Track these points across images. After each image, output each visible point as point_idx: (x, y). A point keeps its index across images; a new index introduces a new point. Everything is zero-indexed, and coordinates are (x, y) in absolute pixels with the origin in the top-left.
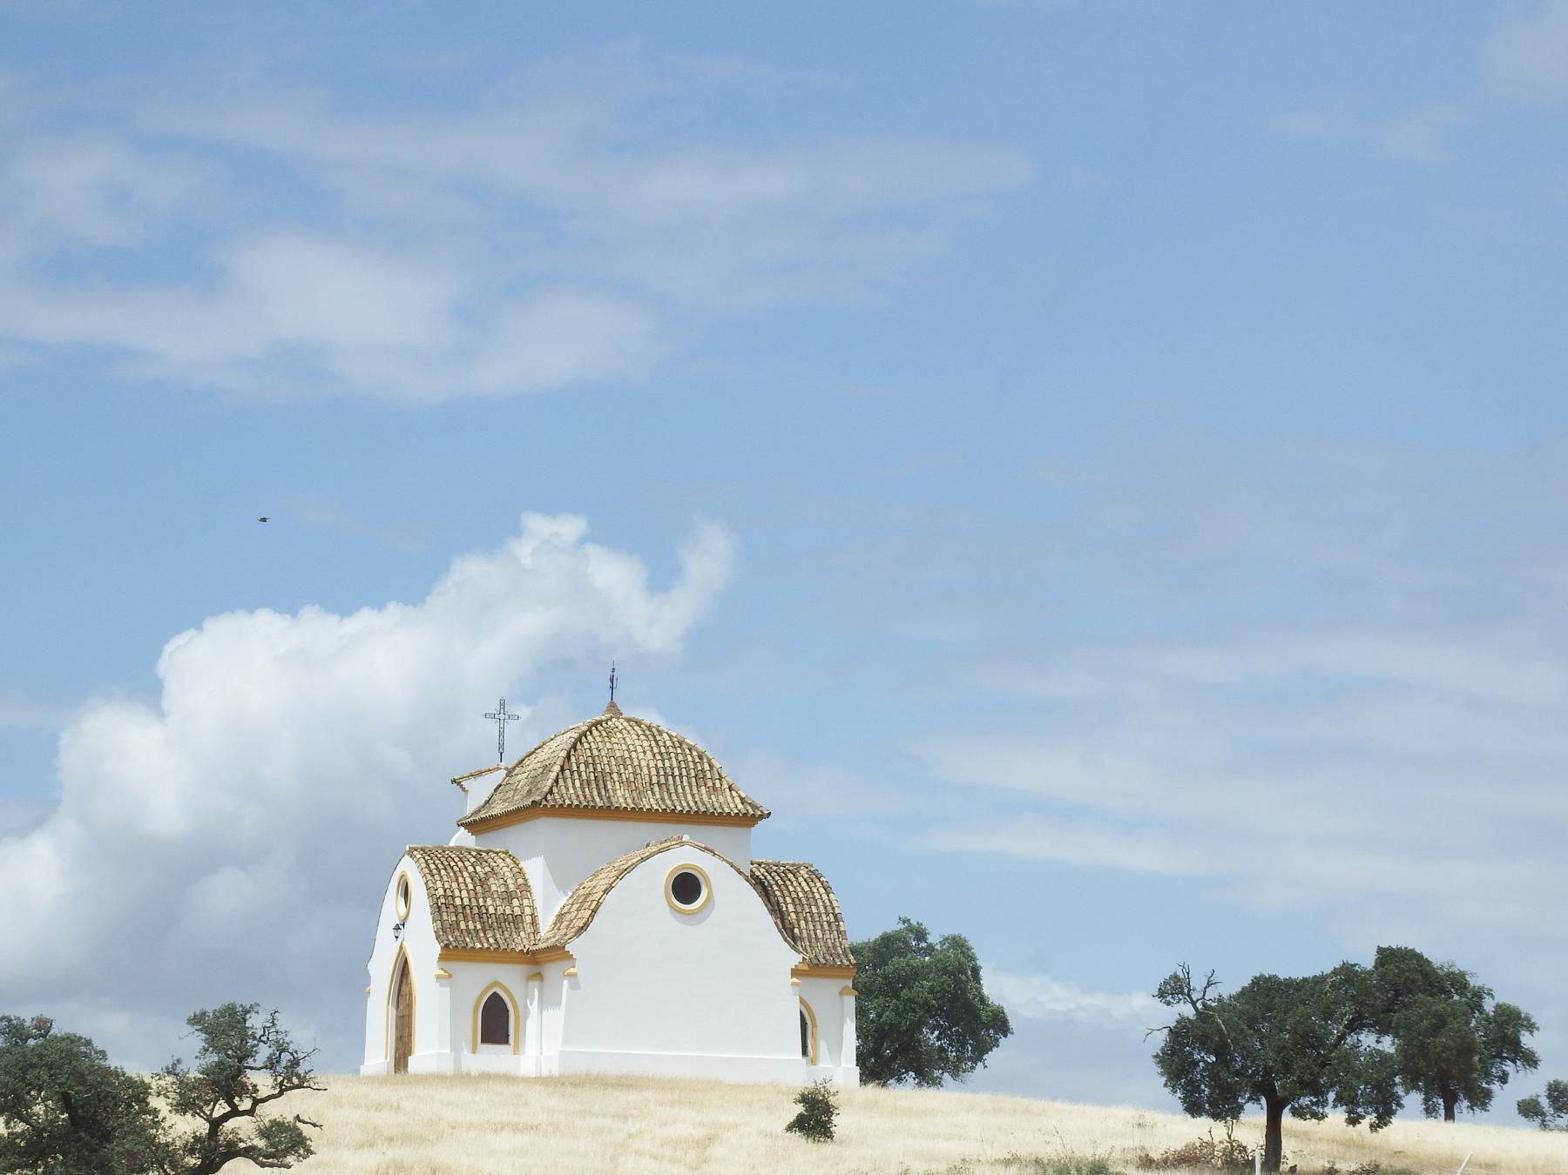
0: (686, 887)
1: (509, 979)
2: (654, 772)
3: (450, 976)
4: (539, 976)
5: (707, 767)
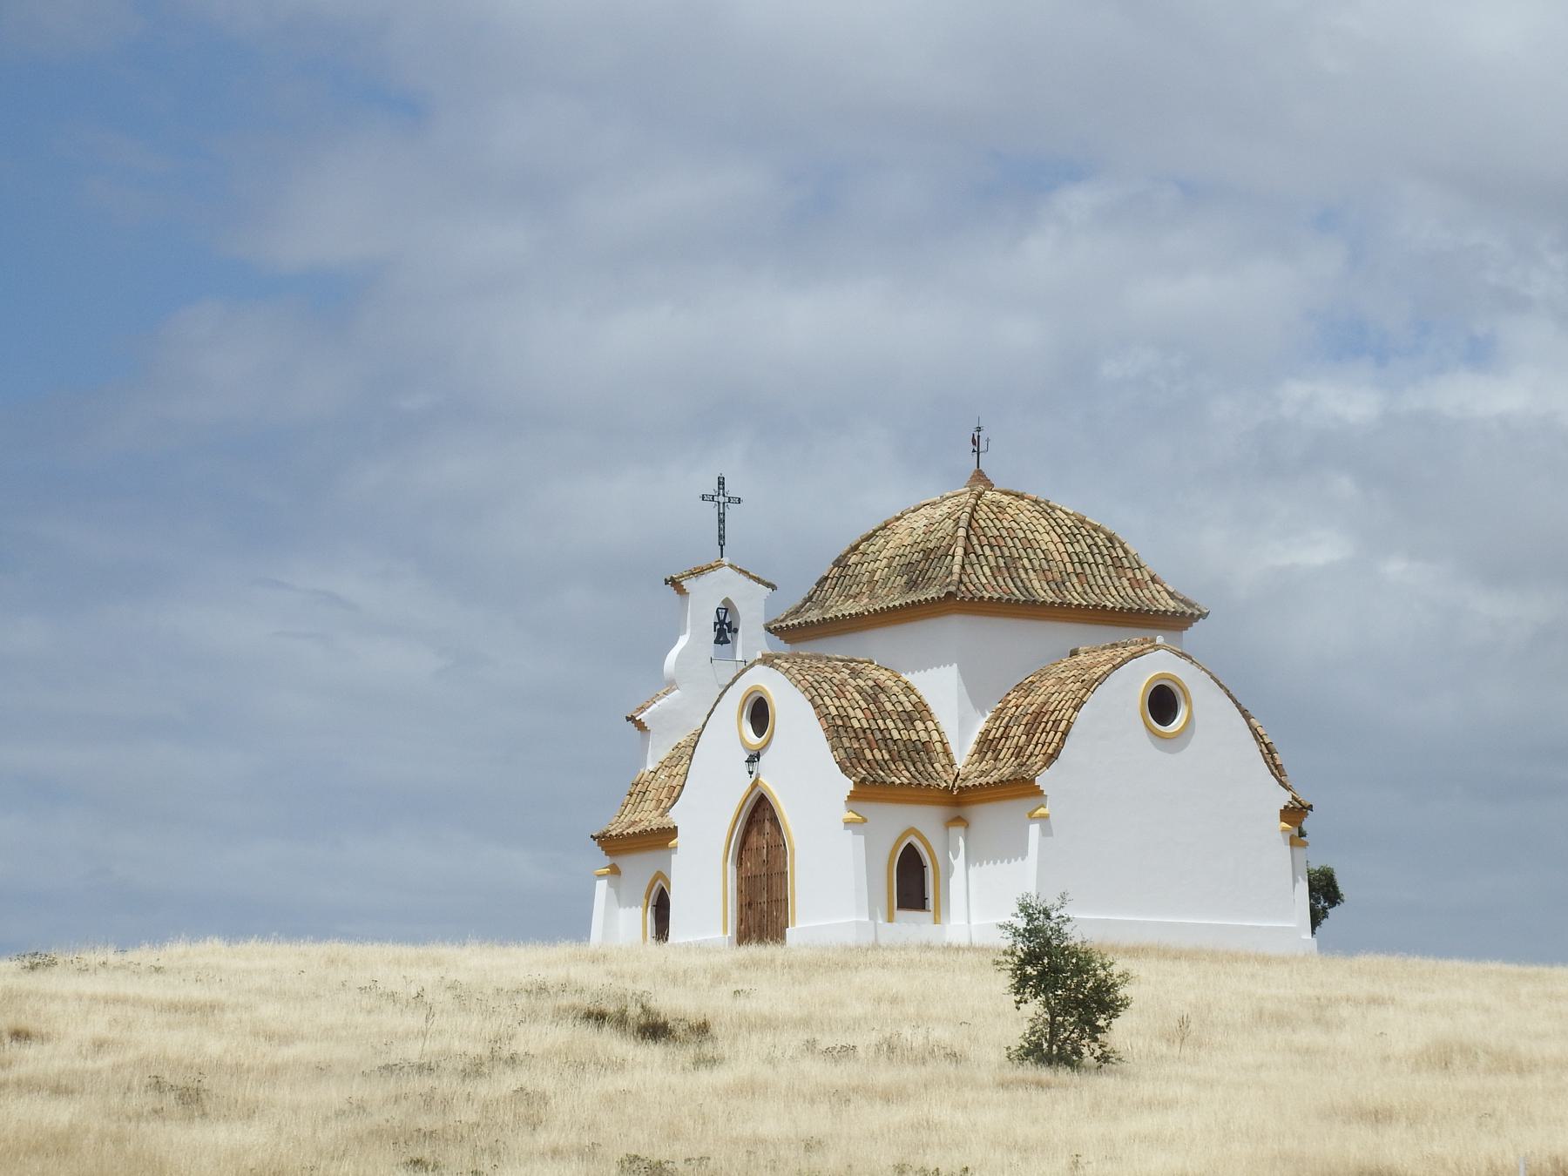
0: (1162, 703)
1: (925, 822)
2: (1067, 559)
3: (865, 820)
4: (959, 820)
5: (1122, 554)
